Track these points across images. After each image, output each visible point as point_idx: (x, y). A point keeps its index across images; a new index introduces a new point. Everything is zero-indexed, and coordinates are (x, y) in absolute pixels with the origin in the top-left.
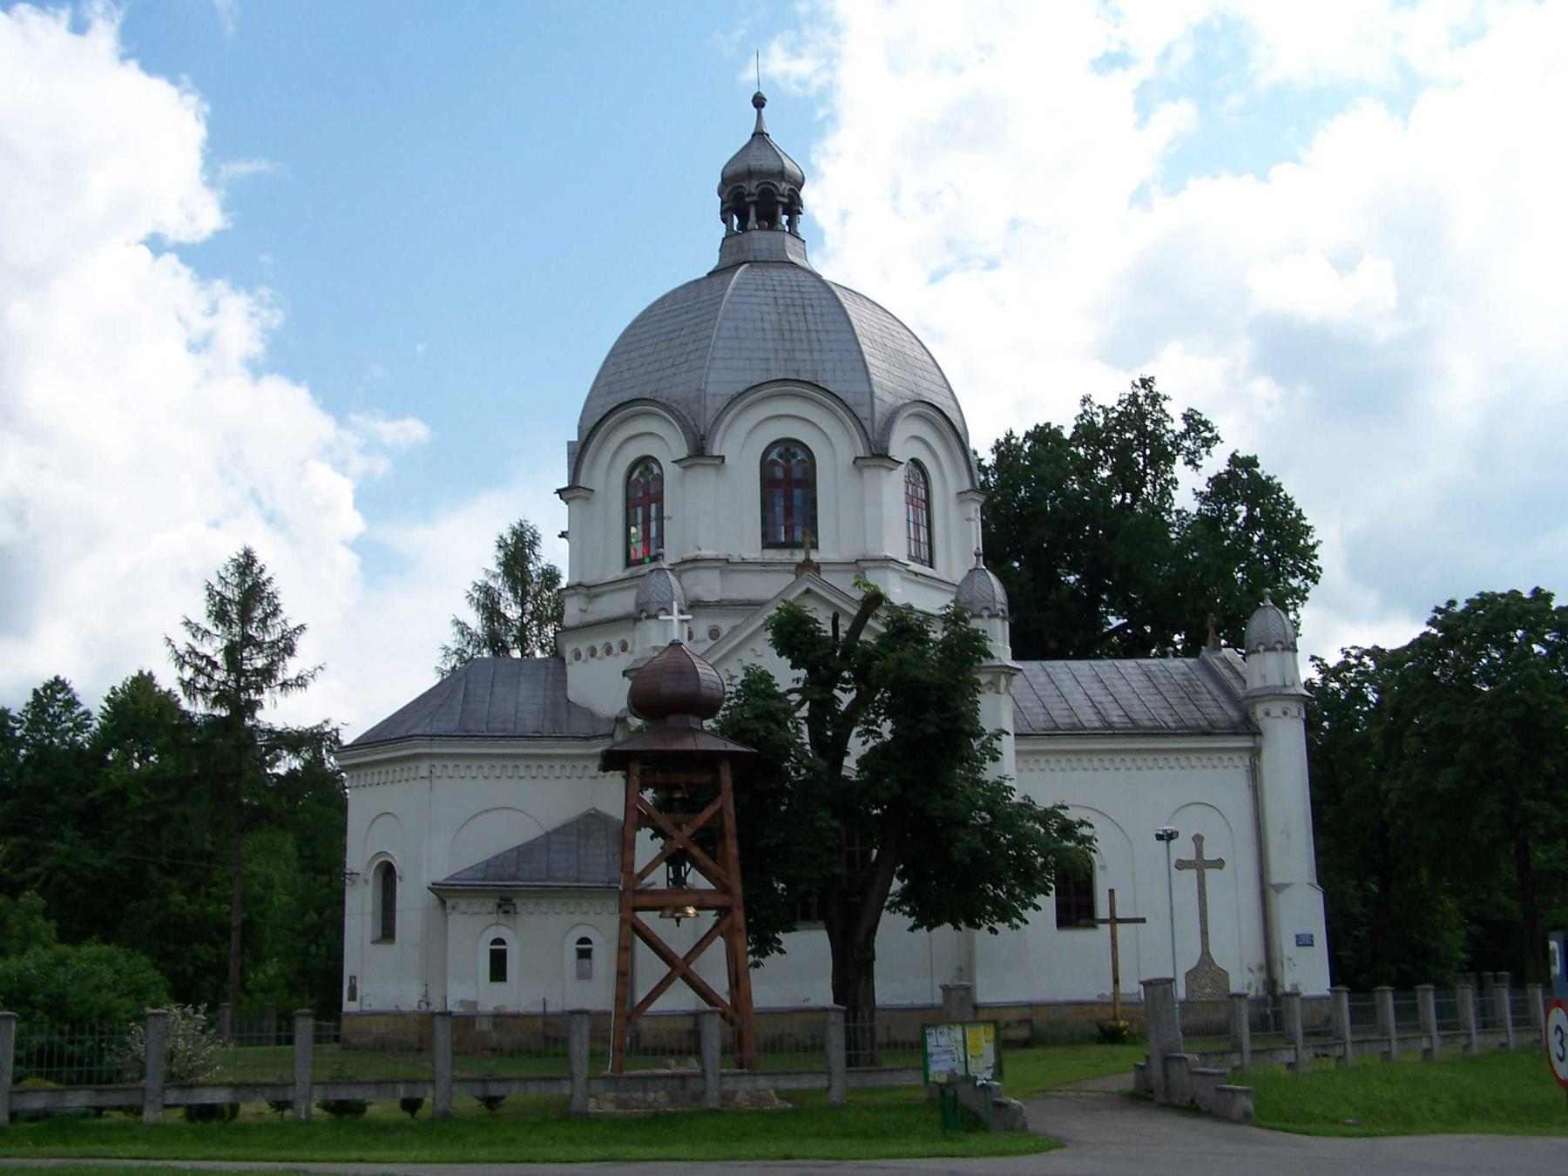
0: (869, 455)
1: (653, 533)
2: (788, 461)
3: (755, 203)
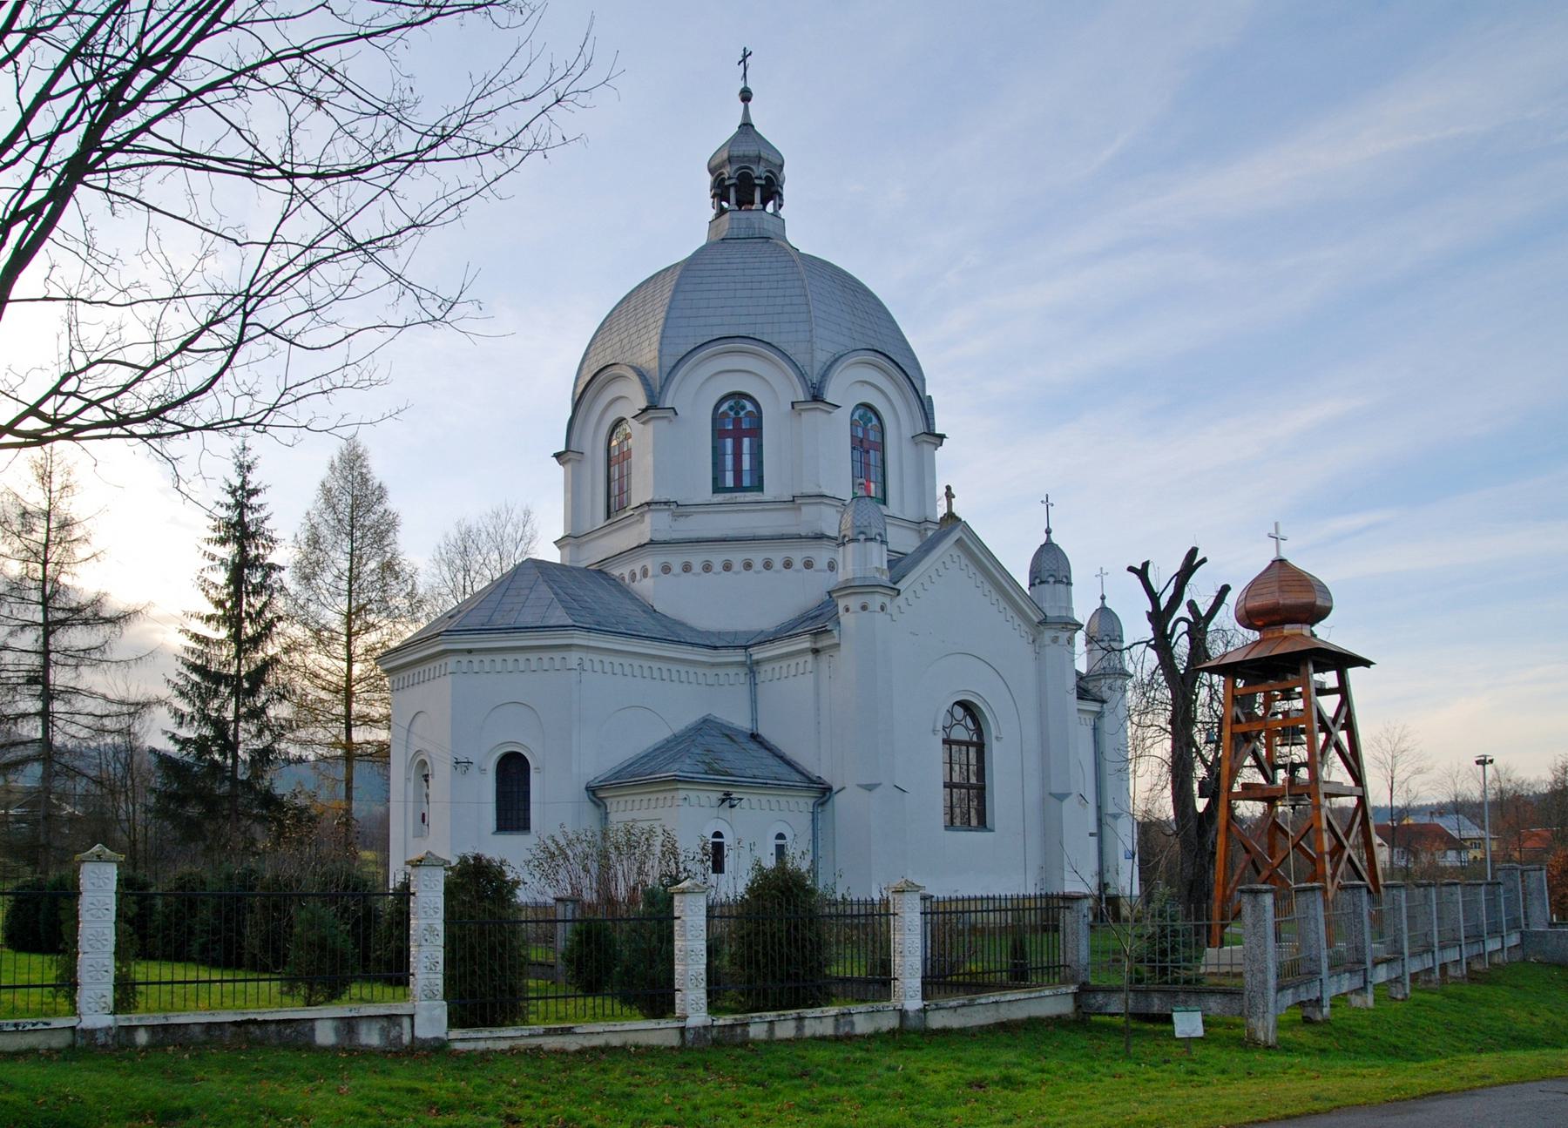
0: (809, 399)
1: (746, 465)
2: (737, 413)
3: (761, 186)
